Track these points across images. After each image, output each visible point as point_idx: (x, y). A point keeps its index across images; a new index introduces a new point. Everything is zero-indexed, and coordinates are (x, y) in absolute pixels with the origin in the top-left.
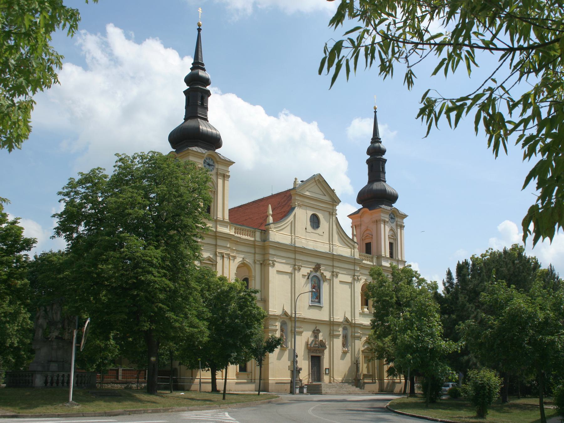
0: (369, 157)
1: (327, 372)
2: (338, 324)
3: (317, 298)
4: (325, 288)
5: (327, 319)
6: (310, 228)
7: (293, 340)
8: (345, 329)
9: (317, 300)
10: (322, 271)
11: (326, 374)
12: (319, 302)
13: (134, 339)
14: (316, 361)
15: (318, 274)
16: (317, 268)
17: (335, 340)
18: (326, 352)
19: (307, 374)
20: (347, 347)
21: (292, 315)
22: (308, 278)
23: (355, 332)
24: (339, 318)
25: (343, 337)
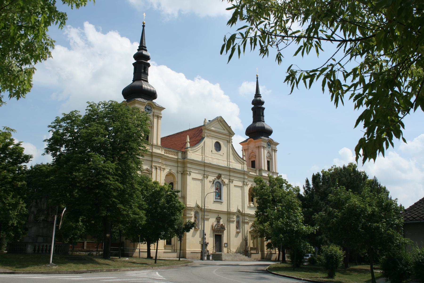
1: (226, 246)
2: (234, 214)
4: (224, 190)
5: (226, 210)
8: (238, 217)
9: (219, 198)
11: (225, 247)
12: (220, 199)
14: (218, 238)
16: (219, 176)
17: (231, 224)
18: (225, 232)
22: (213, 183)
23: (244, 219)
24: (234, 209)
25: (237, 222)
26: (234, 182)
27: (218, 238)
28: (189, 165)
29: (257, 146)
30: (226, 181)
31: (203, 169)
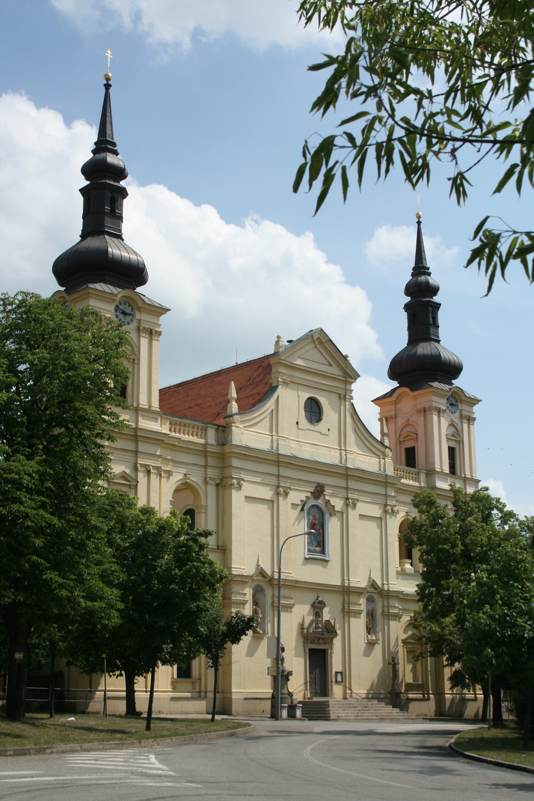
0: (408, 299)
1: (339, 679)
2: (359, 592)
4: (333, 526)
6: (304, 423)
8: (370, 600)
9: (318, 549)
10: (327, 498)
11: (336, 682)
12: (323, 552)
14: (318, 659)
15: (320, 502)
16: (319, 491)
17: (352, 620)
18: (337, 642)
19: (303, 682)
20: (375, 633)
21: (273, 575)
22: (302, 510)
23: (388, 607)
25: (367, 614)
29: (420, 407)
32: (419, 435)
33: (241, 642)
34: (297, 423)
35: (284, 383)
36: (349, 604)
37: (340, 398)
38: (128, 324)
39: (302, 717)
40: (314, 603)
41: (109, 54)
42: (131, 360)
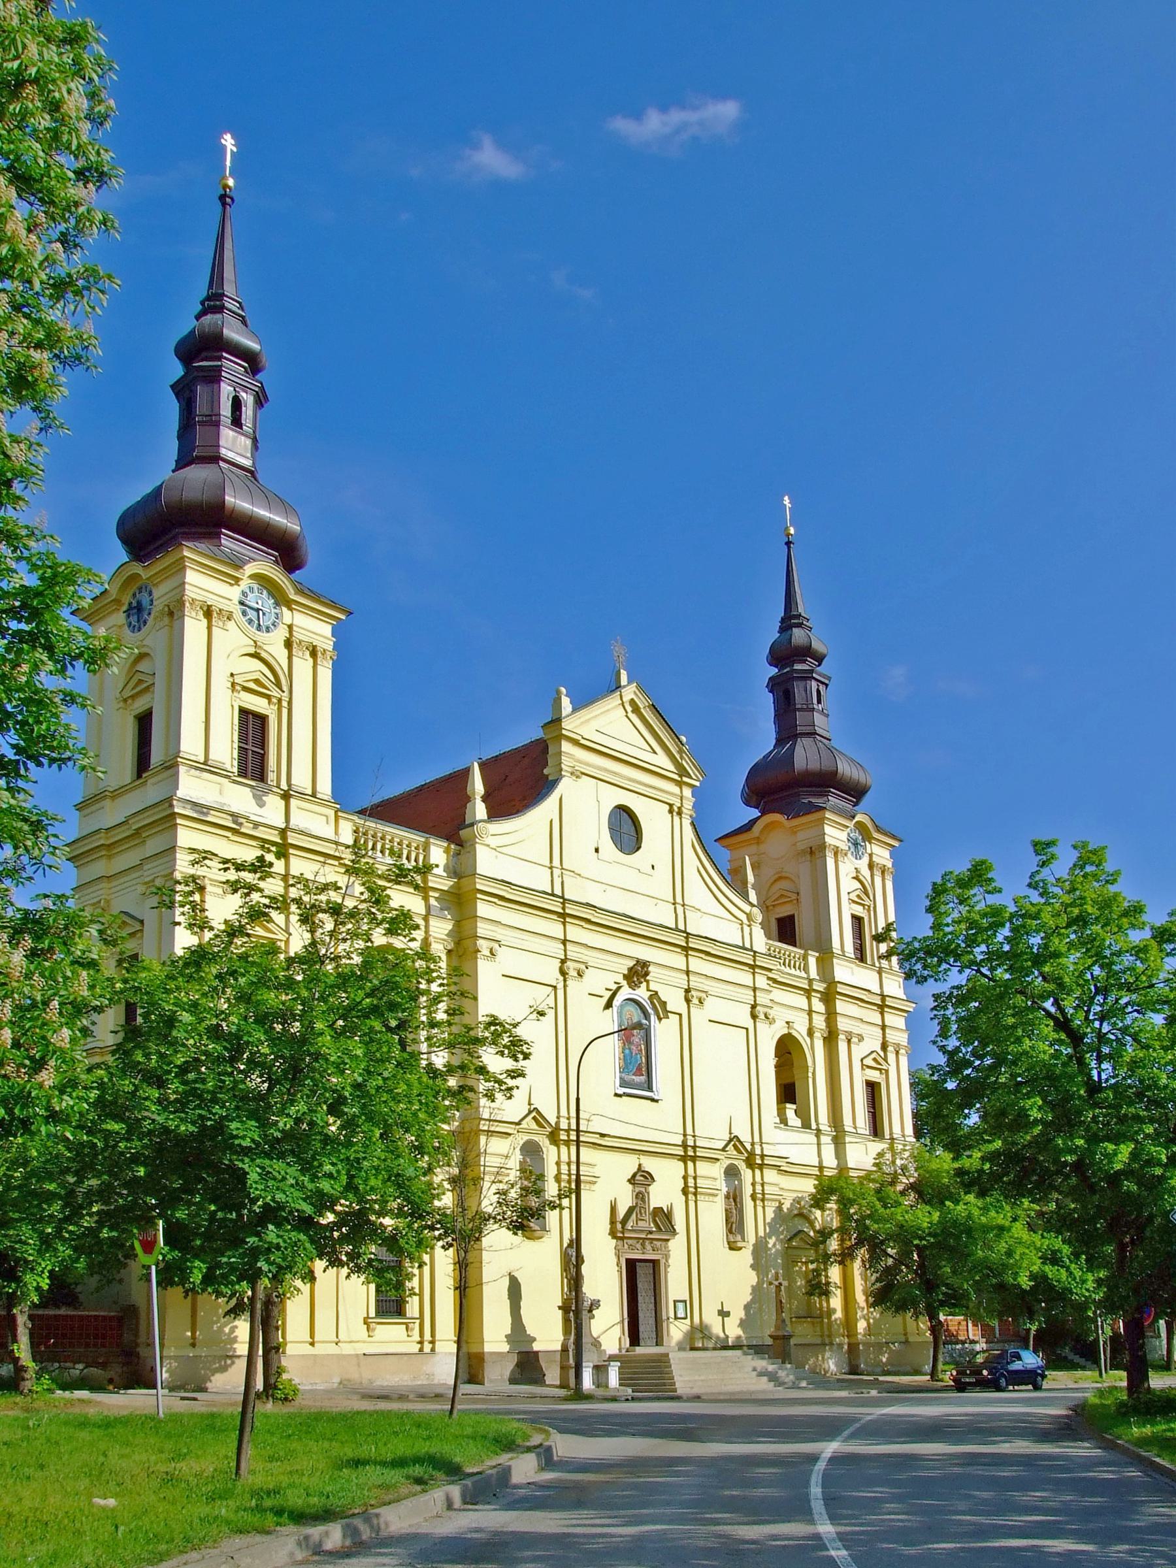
0: (774, 671)
1: (681, 1314)
3: (638, 1072)
4: (664, 1034)
6: (609, 848)
7: (285, 712)
10: (653, 986)
13: (202, 1246)
14: (641, 1279)
15: (642, 994)
16: (638, 973)
18: (677, 1247)
19: (618, 1319)
21: (557, 1123)
22: (609, 1005)
24: (711, 1130)
25: (727, 1197)
26: (709, 1002)
27: (641, 1279)
28: (484, 909)
29: (802, 846)
30: (675, 1001)
31: (556, 929)
32: (802, 893)
33: (750, 1290)
34: (597, 850)
35: (572, 774)
36: (695, 1178)
37: (671, 812)
38: (268, 631)
39: (621, 1385)
40: (634, 1176)
41: (228, 141)
42: (274, 700)
